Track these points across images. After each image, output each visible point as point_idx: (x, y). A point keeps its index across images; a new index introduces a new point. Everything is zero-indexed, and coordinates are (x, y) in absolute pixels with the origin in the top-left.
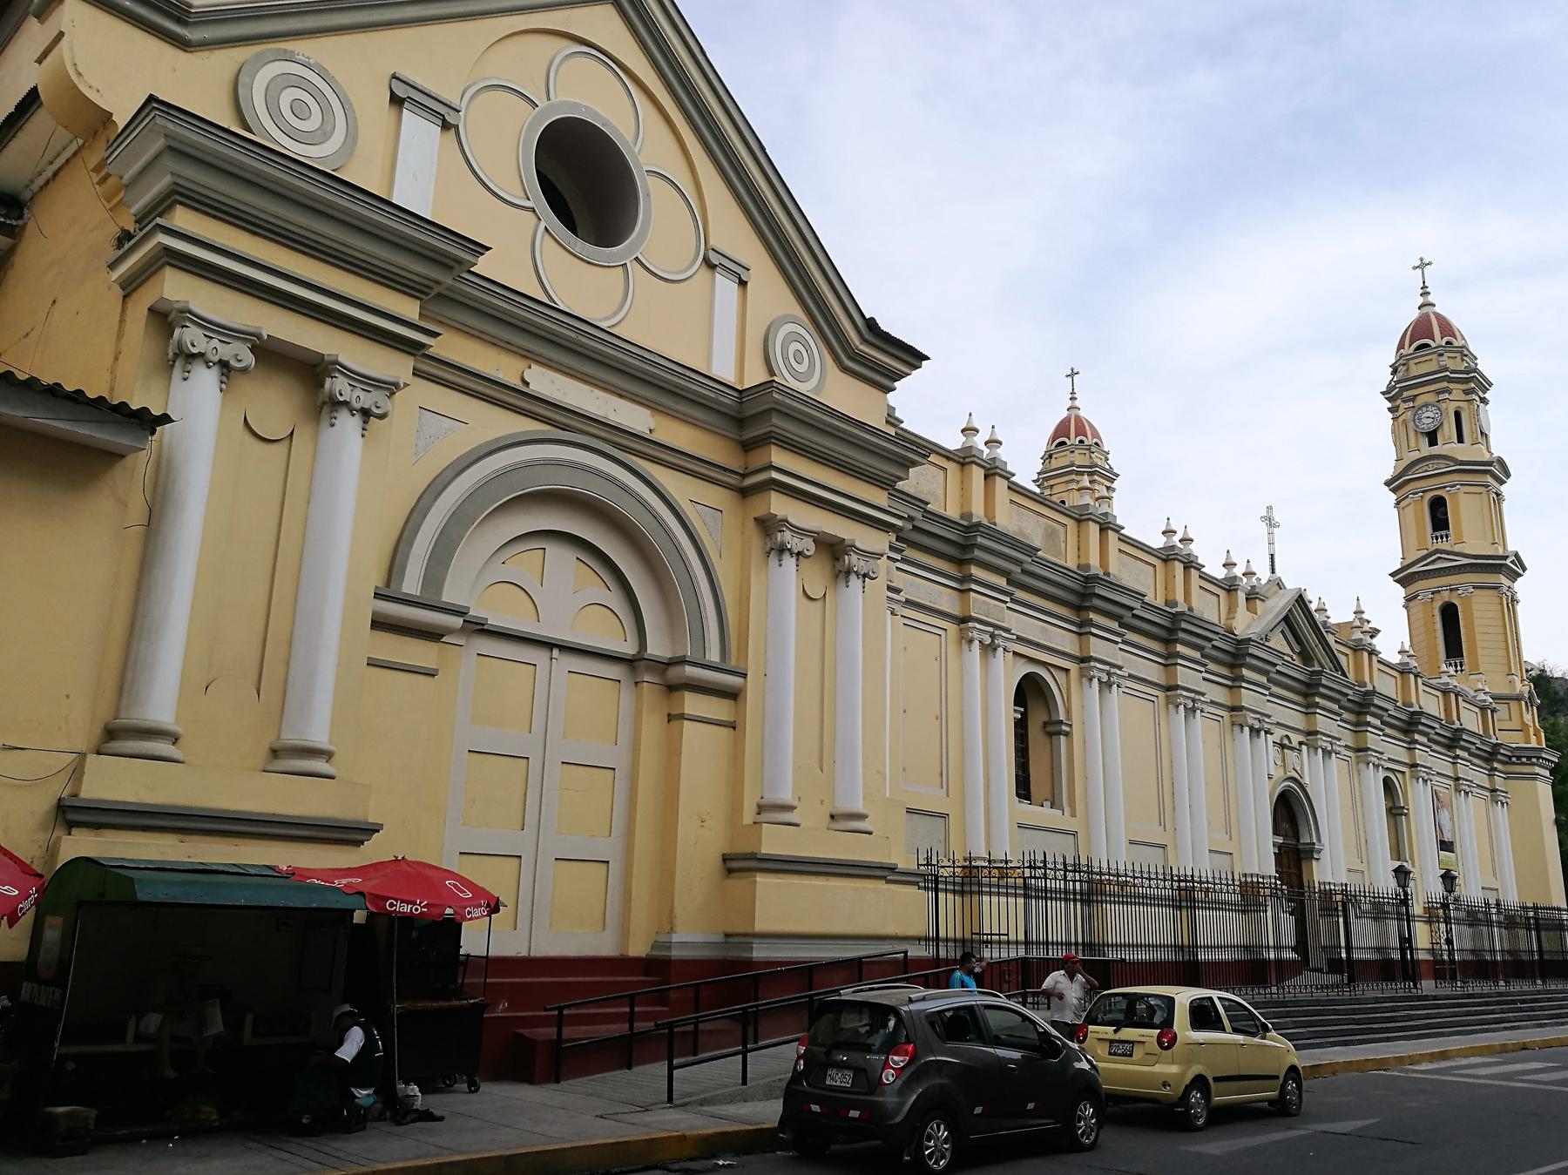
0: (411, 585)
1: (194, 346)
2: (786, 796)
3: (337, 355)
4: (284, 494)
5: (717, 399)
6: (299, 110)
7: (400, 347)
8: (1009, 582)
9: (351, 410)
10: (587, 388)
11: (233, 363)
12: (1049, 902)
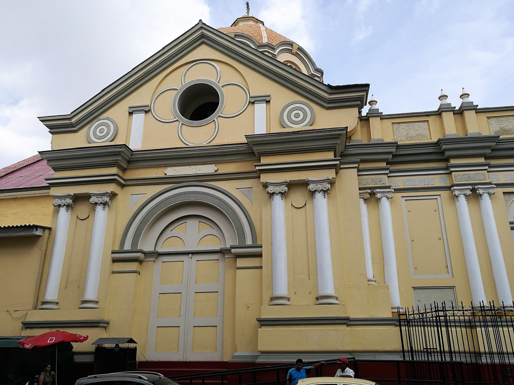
0: (127, 246)
1: (271, 191)
2: (330, 291)
3: (308, 178)
4: (443, 215)
5: (238, 150)
6: (297, 116)
7: (64, 185)
8: (486, 158)
9: (277, 194)
10: (188, 167)
11: (282, 192)
12: (426, 328)
